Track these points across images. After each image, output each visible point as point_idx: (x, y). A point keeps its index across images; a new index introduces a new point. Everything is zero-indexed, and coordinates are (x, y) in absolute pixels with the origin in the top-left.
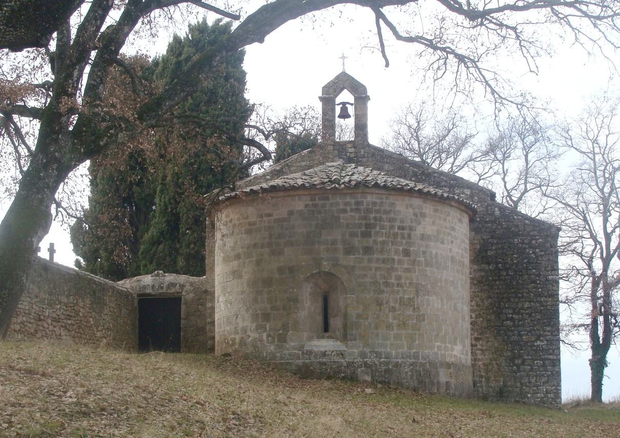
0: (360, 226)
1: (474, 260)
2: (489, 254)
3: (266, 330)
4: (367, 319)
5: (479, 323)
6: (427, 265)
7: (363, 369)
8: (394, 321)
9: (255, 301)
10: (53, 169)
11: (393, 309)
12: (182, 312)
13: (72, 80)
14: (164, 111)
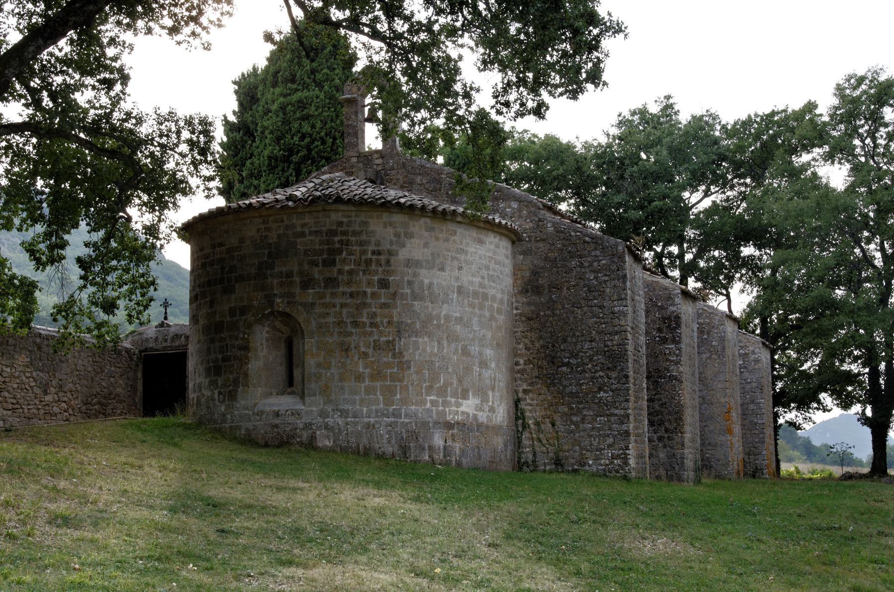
1: (522, 290)
7: (323, 431)
8: (366, 371)
11: (365, 355)
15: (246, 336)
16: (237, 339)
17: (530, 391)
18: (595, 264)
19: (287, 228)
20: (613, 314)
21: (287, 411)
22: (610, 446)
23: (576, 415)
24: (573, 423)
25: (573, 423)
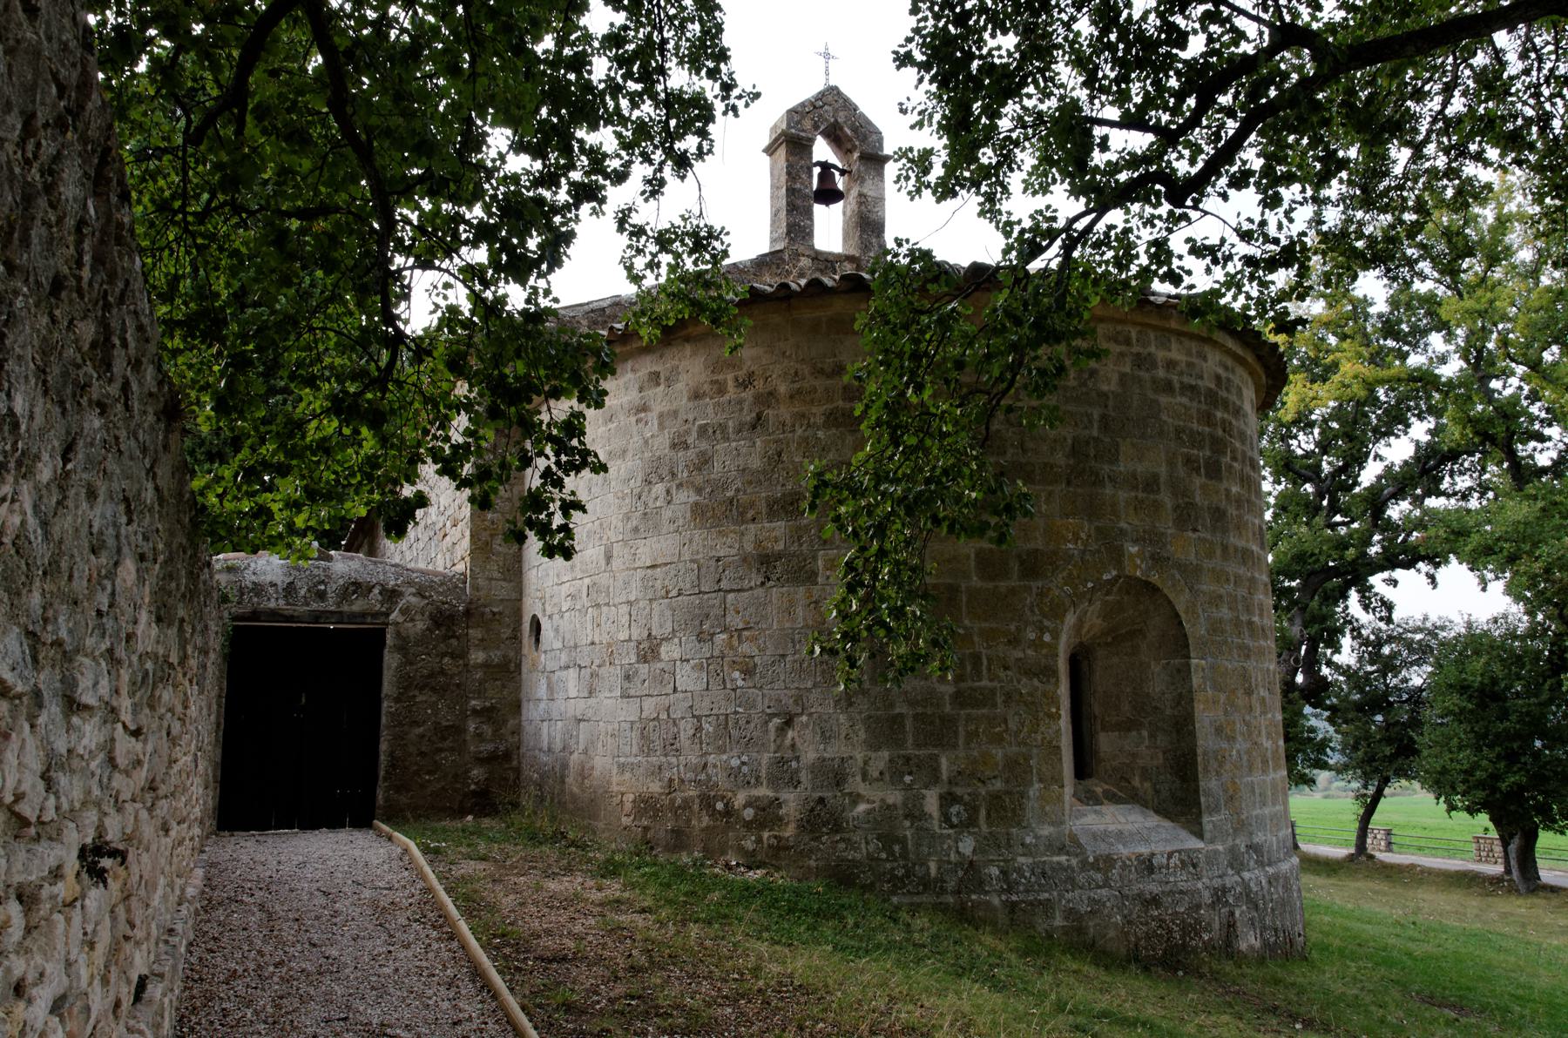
3: (935, 778)
15: (1047, 638)
16: (1014, 641)
21: (1170, 855)
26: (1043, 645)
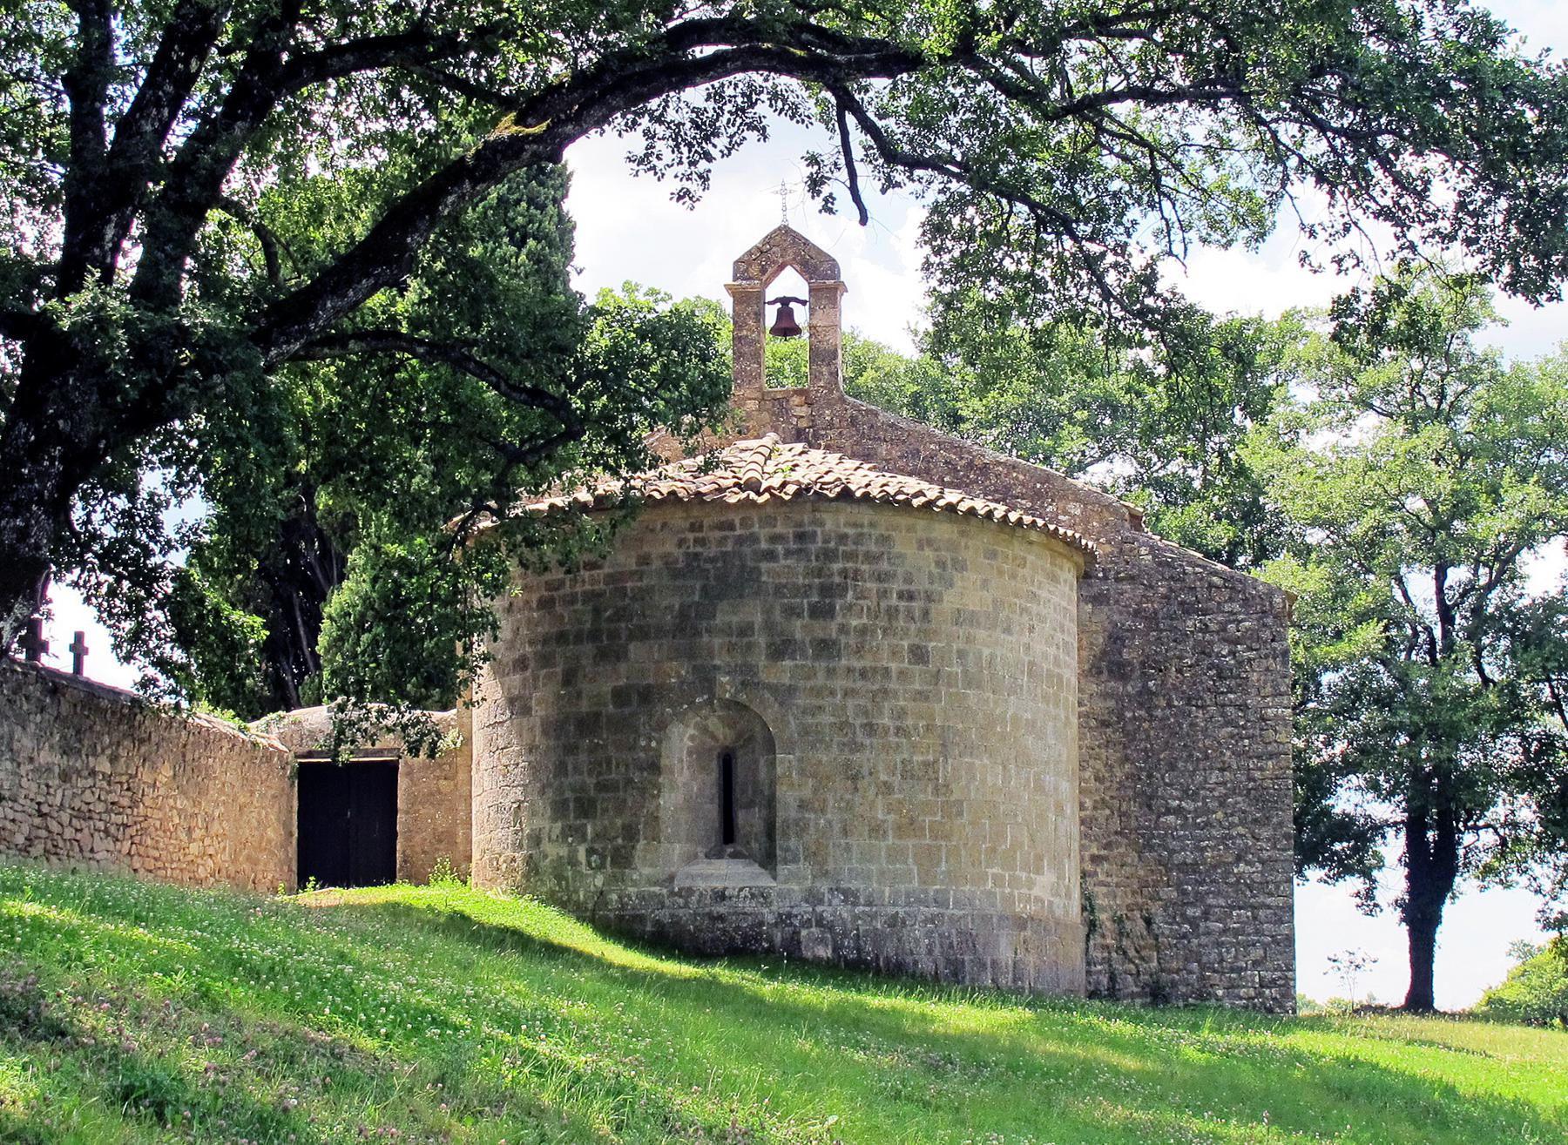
0: (806, 591)
2: (1125, 656)
3: (584, 839)
4: (823, 811)
5: (1102, 820)
6: (969, 685)
9: (561, 770)
10: (52, 460)
11: (887, 788)
12: (399, 793)
13: (102, 247)
14: (321, 322)
15: (654, 744)
17: (1105, 858)
18: (1231, 627)
19: (740, 541)
20: (1264, 720)
21: (741, 889)
22: (1256, 963)
23: (1192, 904)
24: (1186, 919)
25: (1186, 919)
26: (651, 749)
